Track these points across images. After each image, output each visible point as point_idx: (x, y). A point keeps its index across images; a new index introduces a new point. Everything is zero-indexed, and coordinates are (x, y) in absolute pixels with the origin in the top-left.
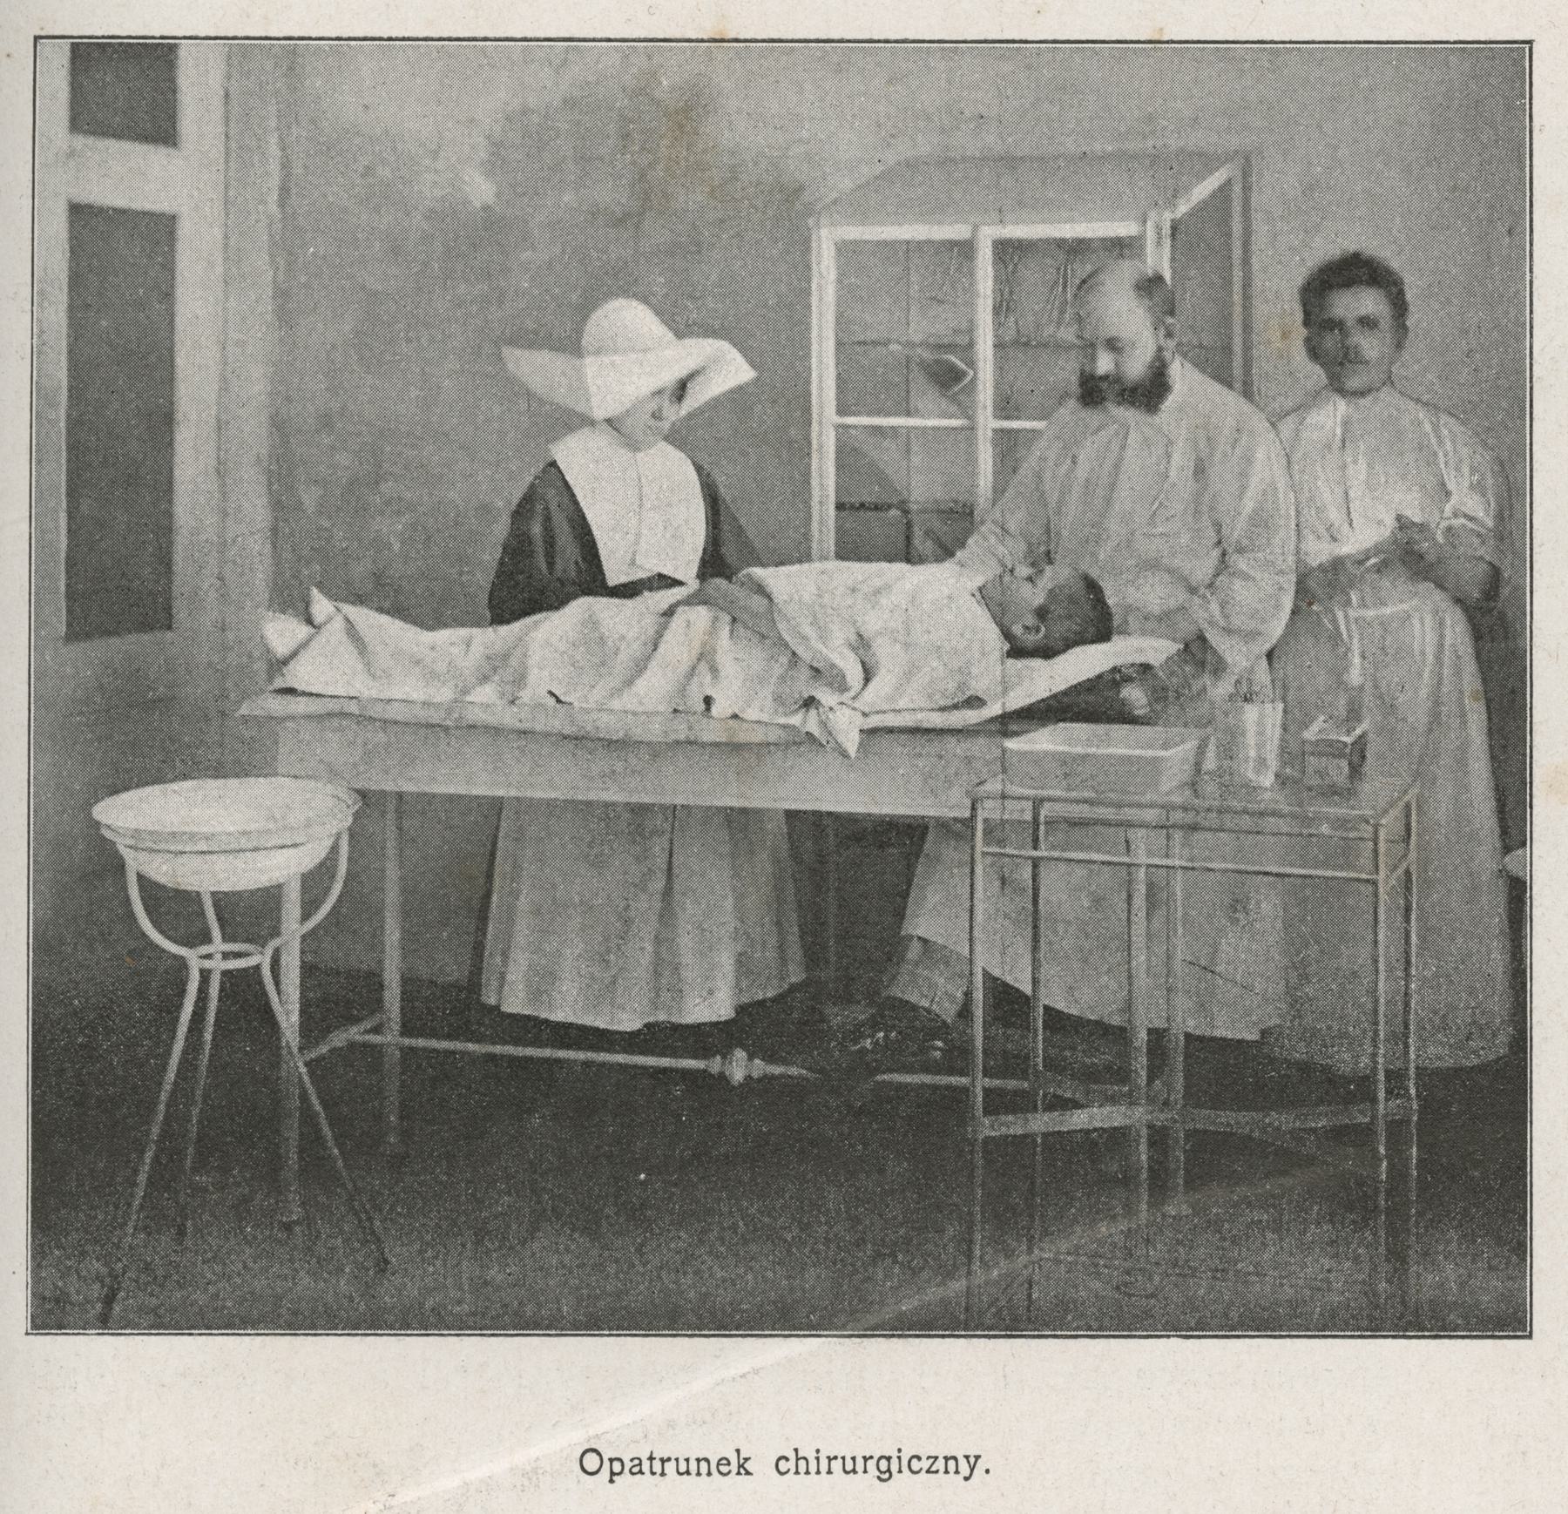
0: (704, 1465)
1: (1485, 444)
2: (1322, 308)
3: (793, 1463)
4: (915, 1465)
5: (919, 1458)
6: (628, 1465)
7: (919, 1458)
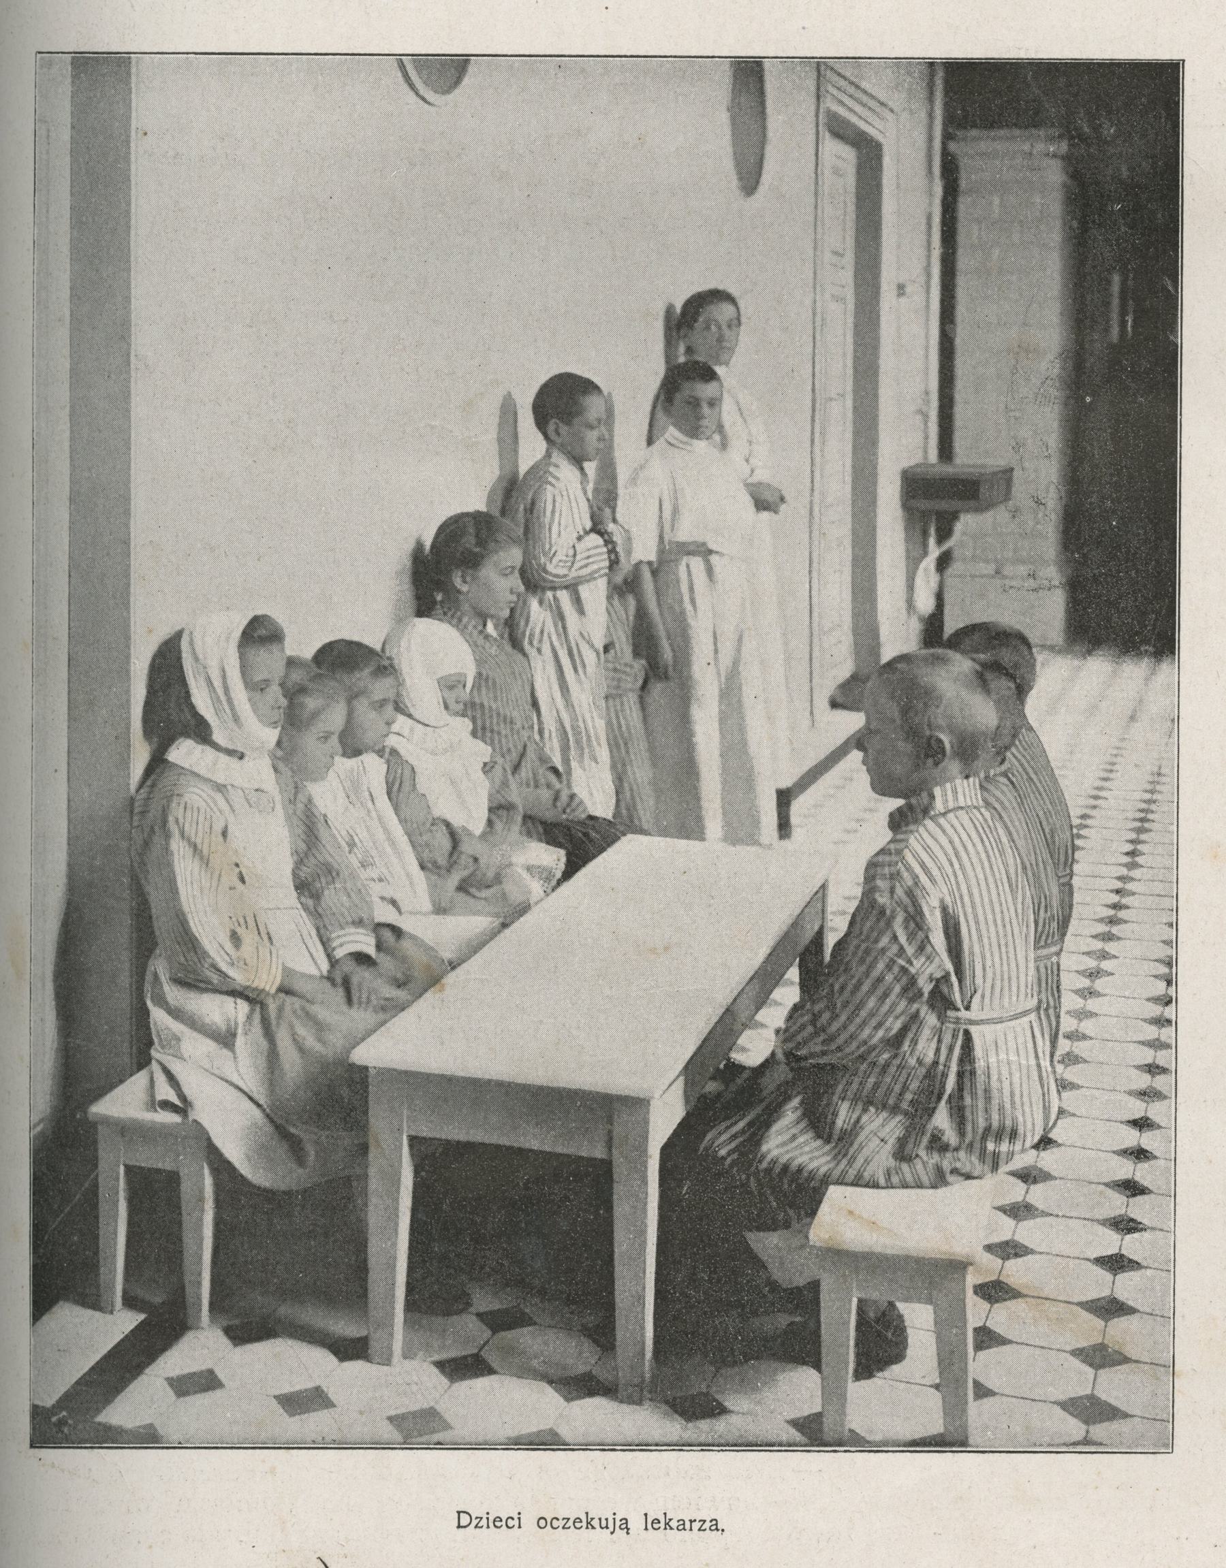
4: (555, 1523)
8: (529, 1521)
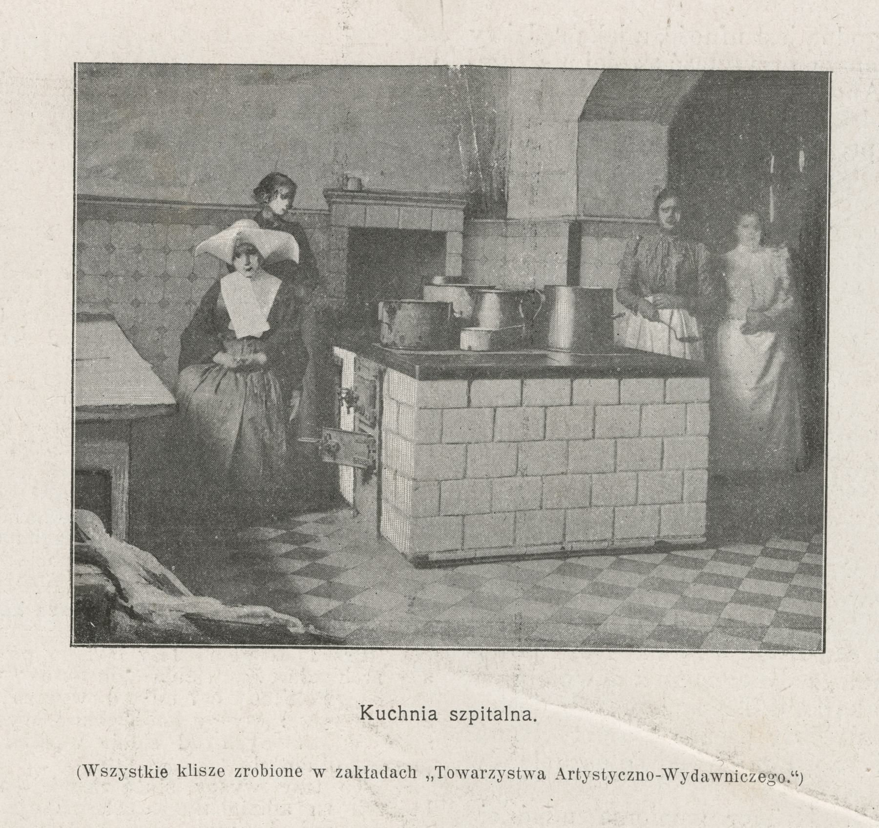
0: (415, 714)
8: (443, 715)
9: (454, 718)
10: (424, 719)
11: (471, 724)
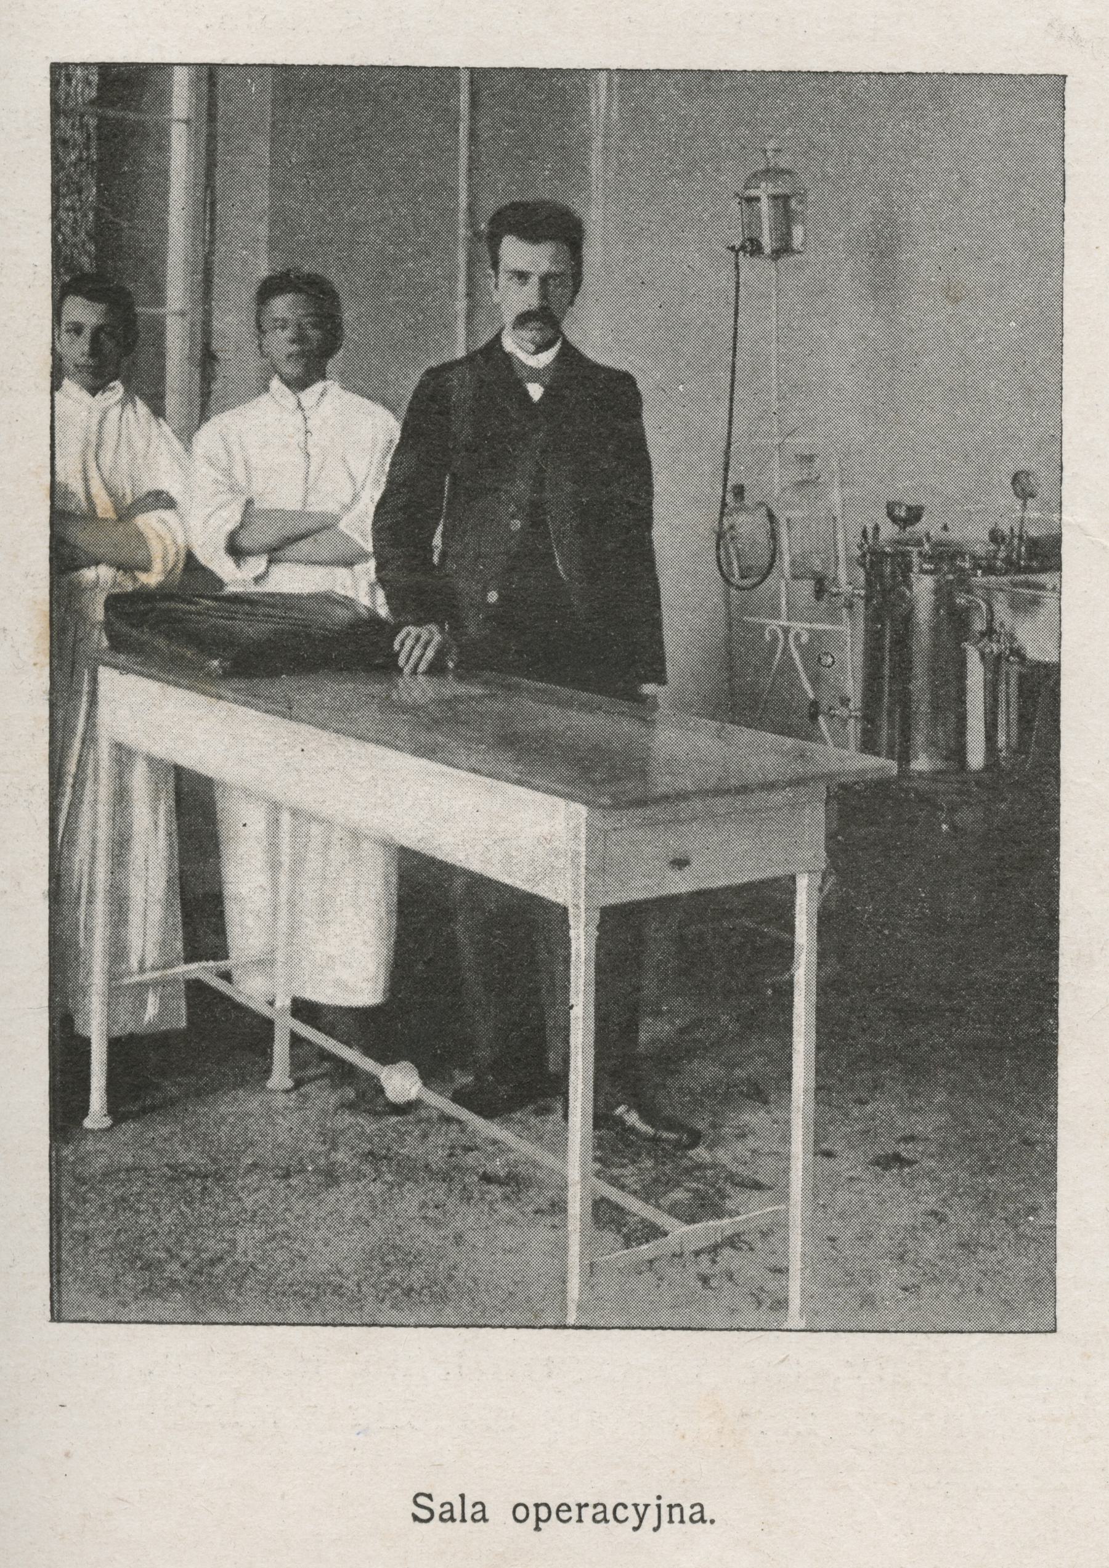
0: (676, 1511)
1: (341, 670)
2: (938, 581)
3: (538, 1515)
5: (625, 1507)
6: (688, 1512)
7: (625, 1507)
9: (424, 1514)
10: (682, 1521)
11: (537, 1529)
